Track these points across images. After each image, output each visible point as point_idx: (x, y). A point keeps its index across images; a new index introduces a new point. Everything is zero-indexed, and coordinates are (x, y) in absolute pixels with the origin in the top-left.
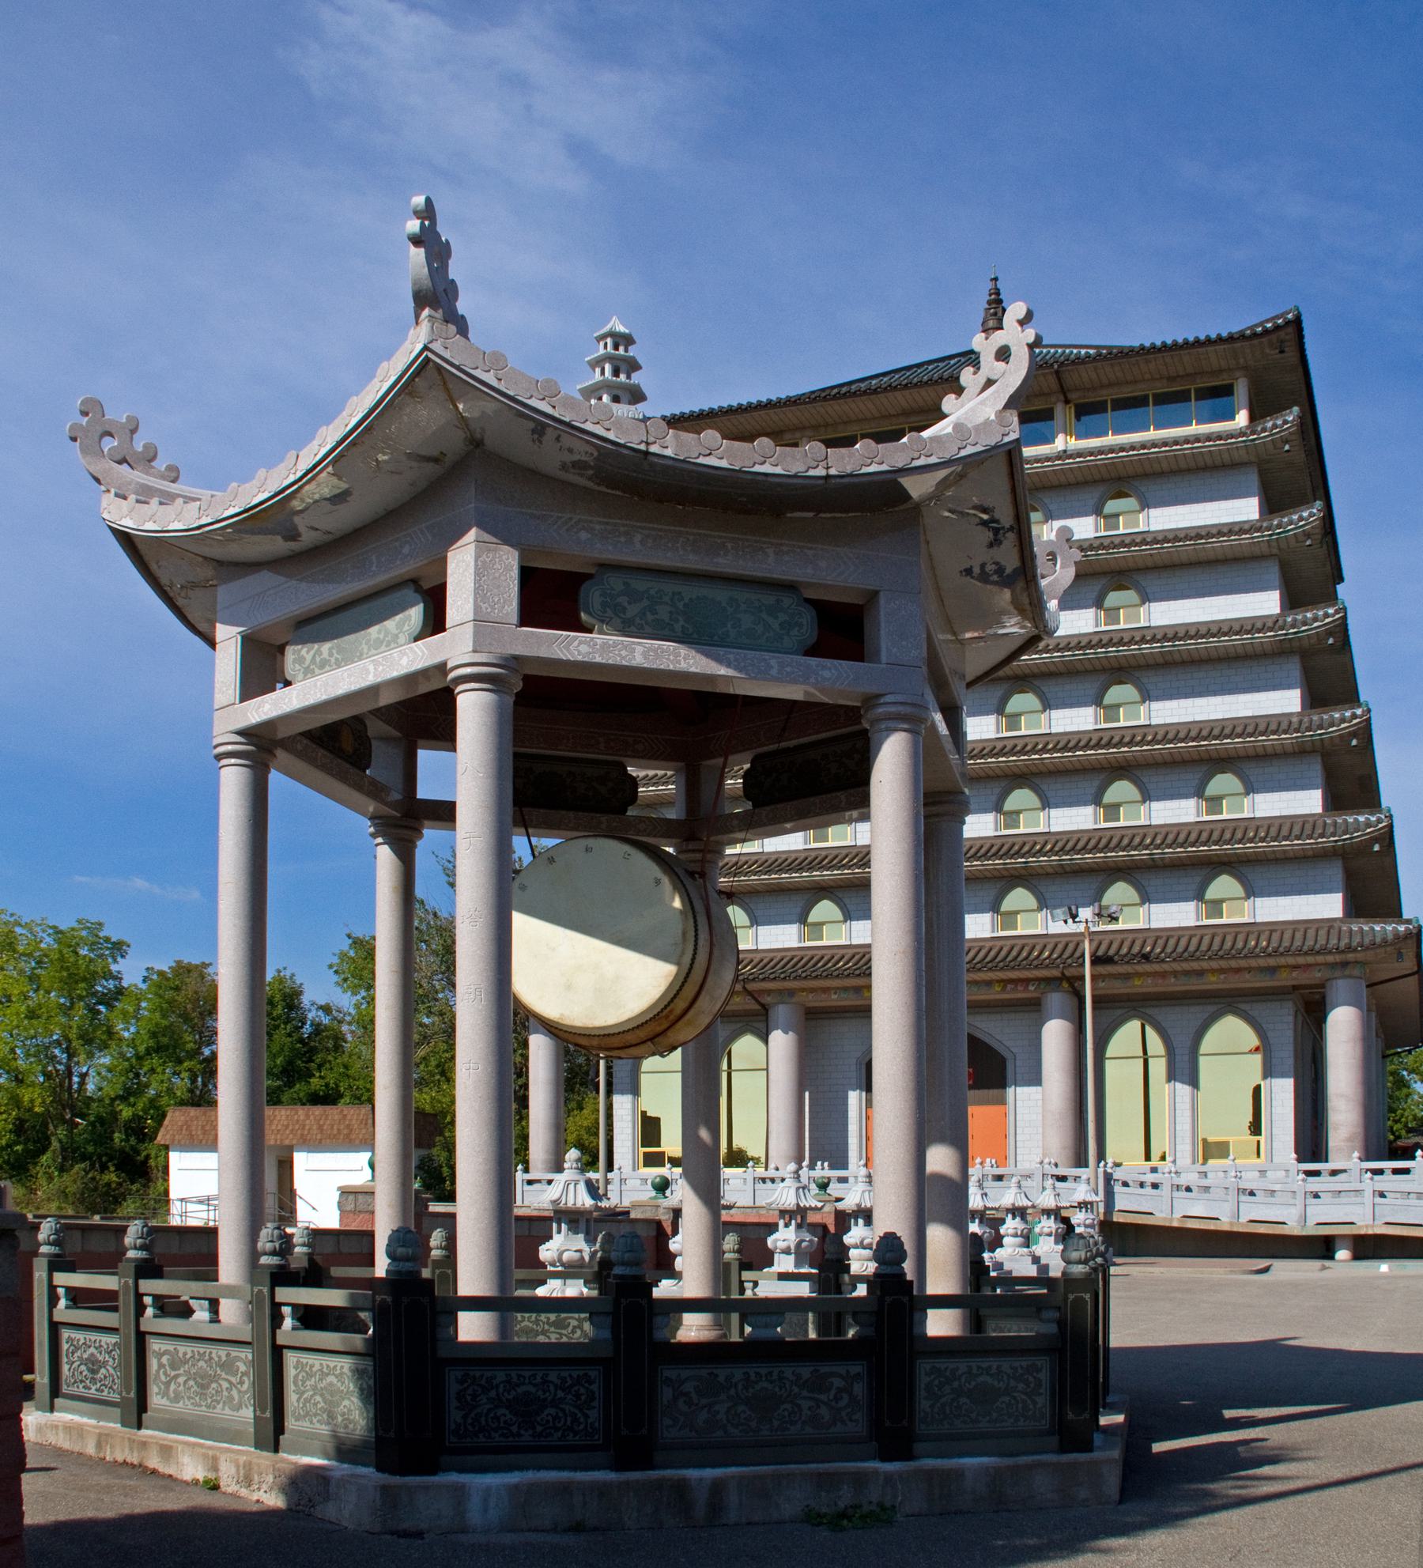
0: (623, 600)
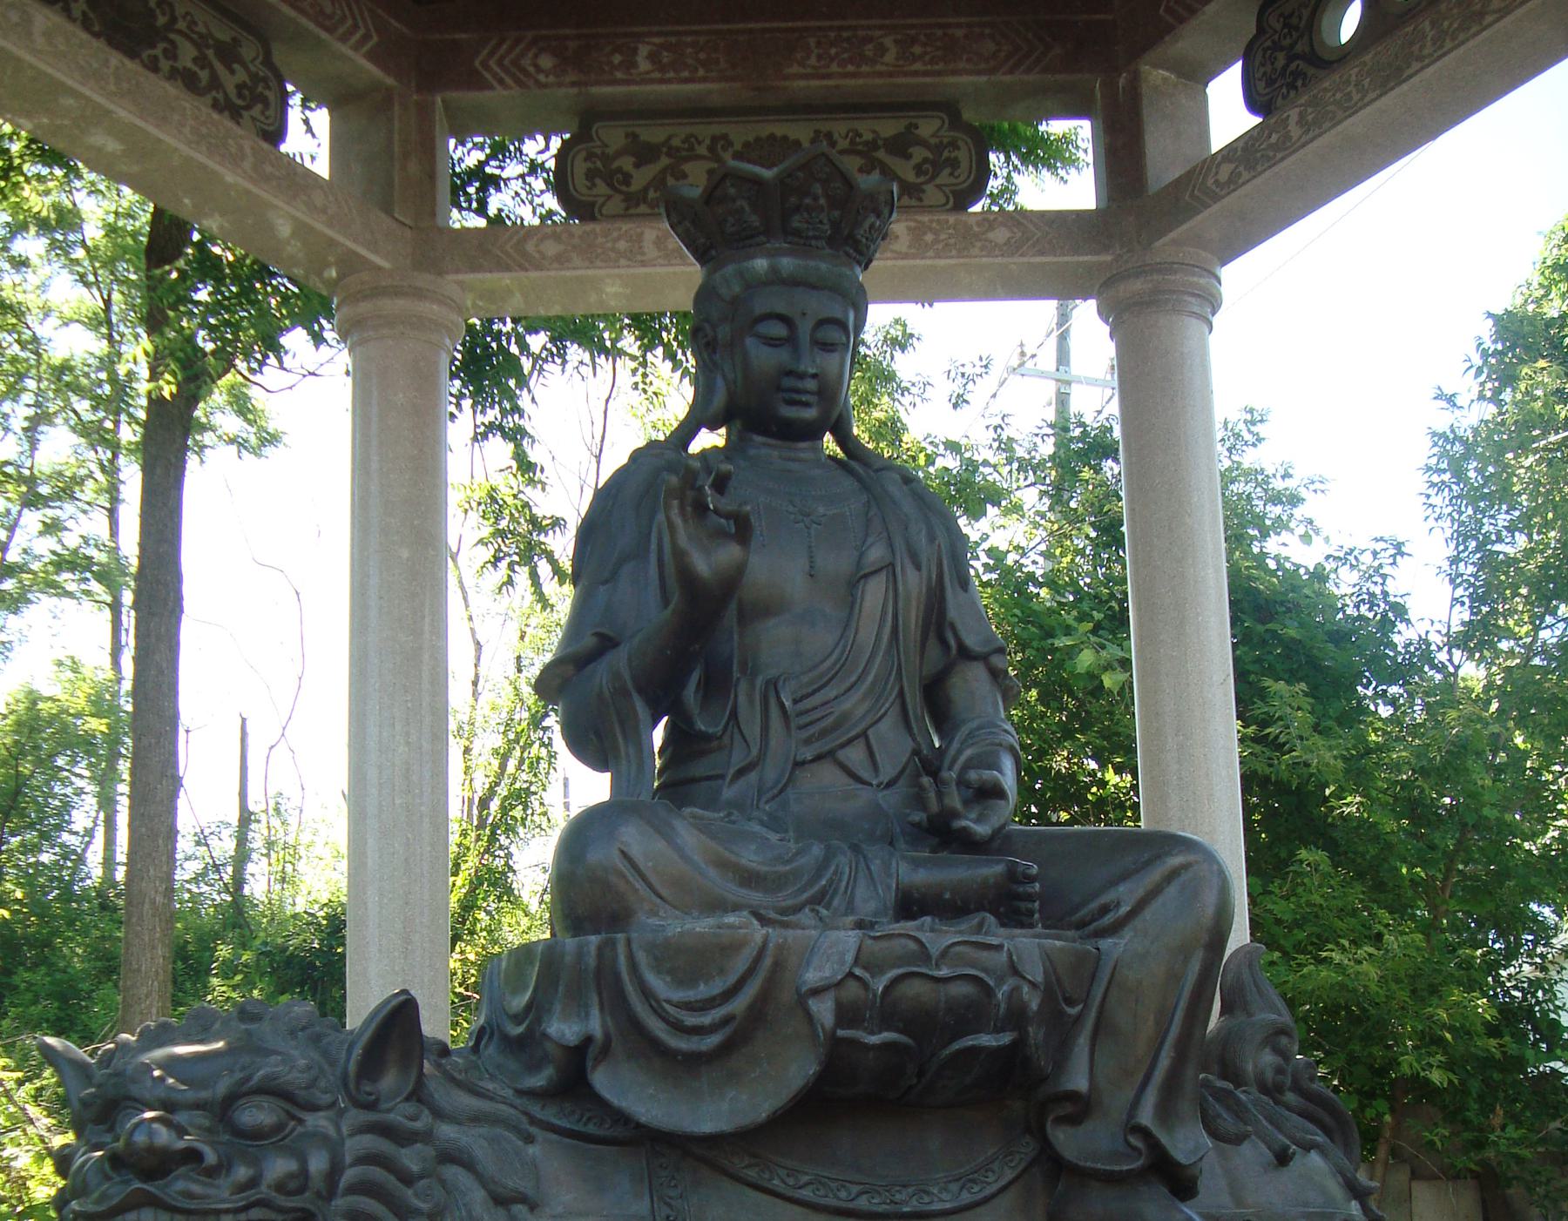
0: (627, 163)
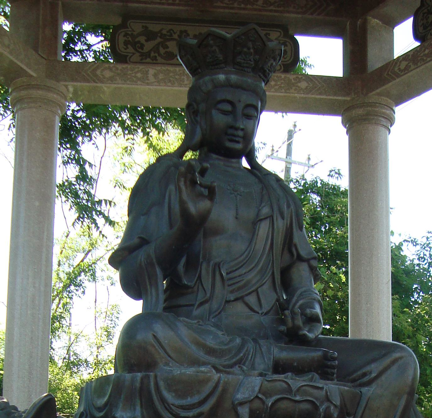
0: (142, 39)
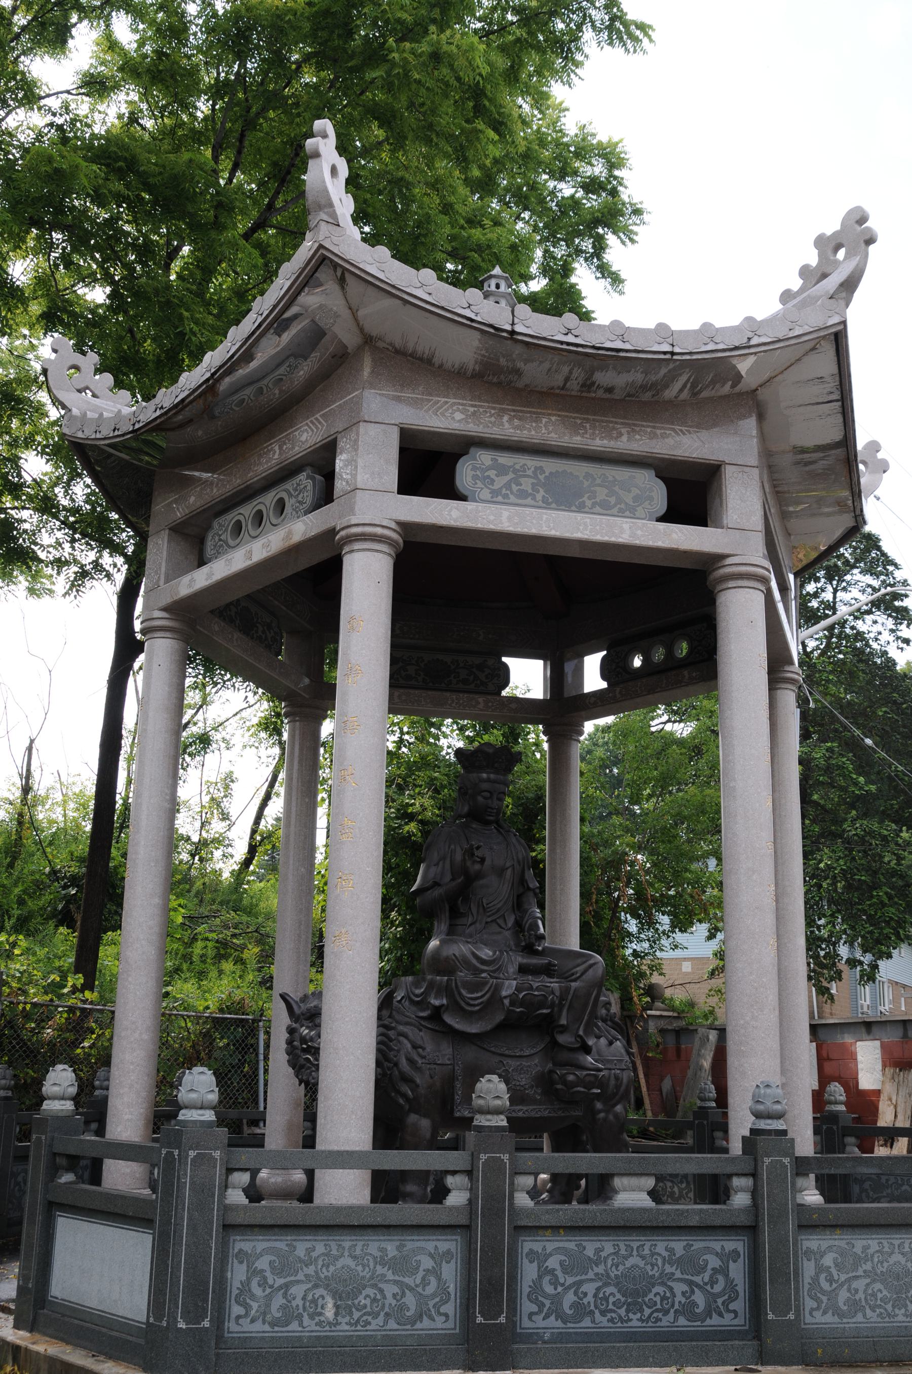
0: (492, 473)
